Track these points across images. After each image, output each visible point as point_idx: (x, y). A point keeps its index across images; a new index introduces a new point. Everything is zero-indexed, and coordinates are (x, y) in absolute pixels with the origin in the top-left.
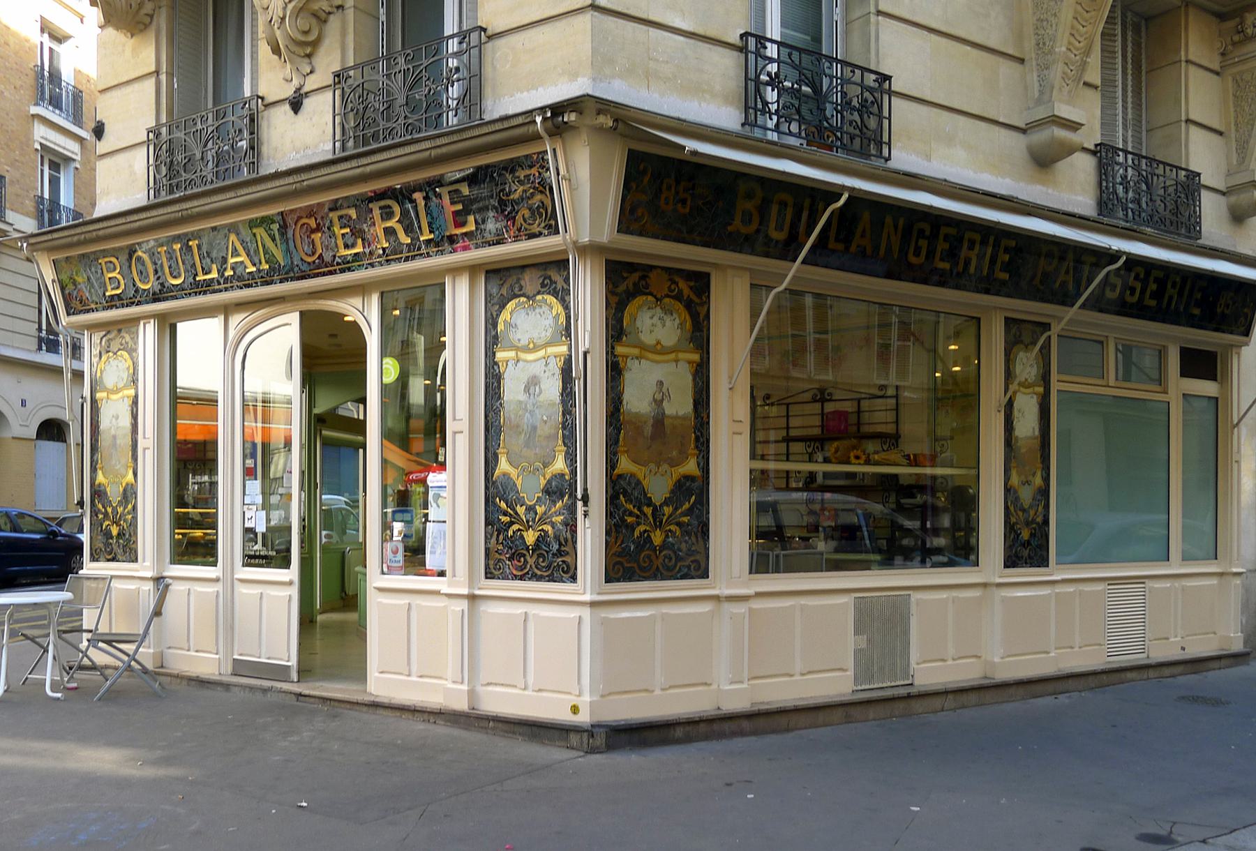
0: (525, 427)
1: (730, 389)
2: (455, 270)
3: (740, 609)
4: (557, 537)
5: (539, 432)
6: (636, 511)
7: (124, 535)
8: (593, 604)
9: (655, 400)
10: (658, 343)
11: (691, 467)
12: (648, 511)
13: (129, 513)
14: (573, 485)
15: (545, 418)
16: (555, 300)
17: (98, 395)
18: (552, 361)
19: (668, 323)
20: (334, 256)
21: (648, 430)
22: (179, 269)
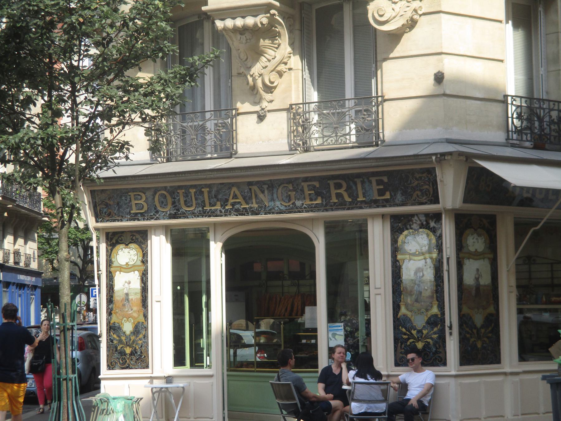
0: (415, 292)
1: (508, 271)
2: (373, 216)
3: (516, 379)
4: (434, 345)
5: (423, 295)
6: (470, 331)
7: (136, 353)
8: (456, 376)
9: (476, 278)
10: (476, 250)
11: (491, 309)
12: (475, 331)
13: (140, 339)
14: (443, 321)
15: (426, 288)
16: (429, 232)
17: (399, 257)
18: (429, 261)
19: (480, 241)
20: (303, 204)
21: (473, 292)
22: (192, 202)
